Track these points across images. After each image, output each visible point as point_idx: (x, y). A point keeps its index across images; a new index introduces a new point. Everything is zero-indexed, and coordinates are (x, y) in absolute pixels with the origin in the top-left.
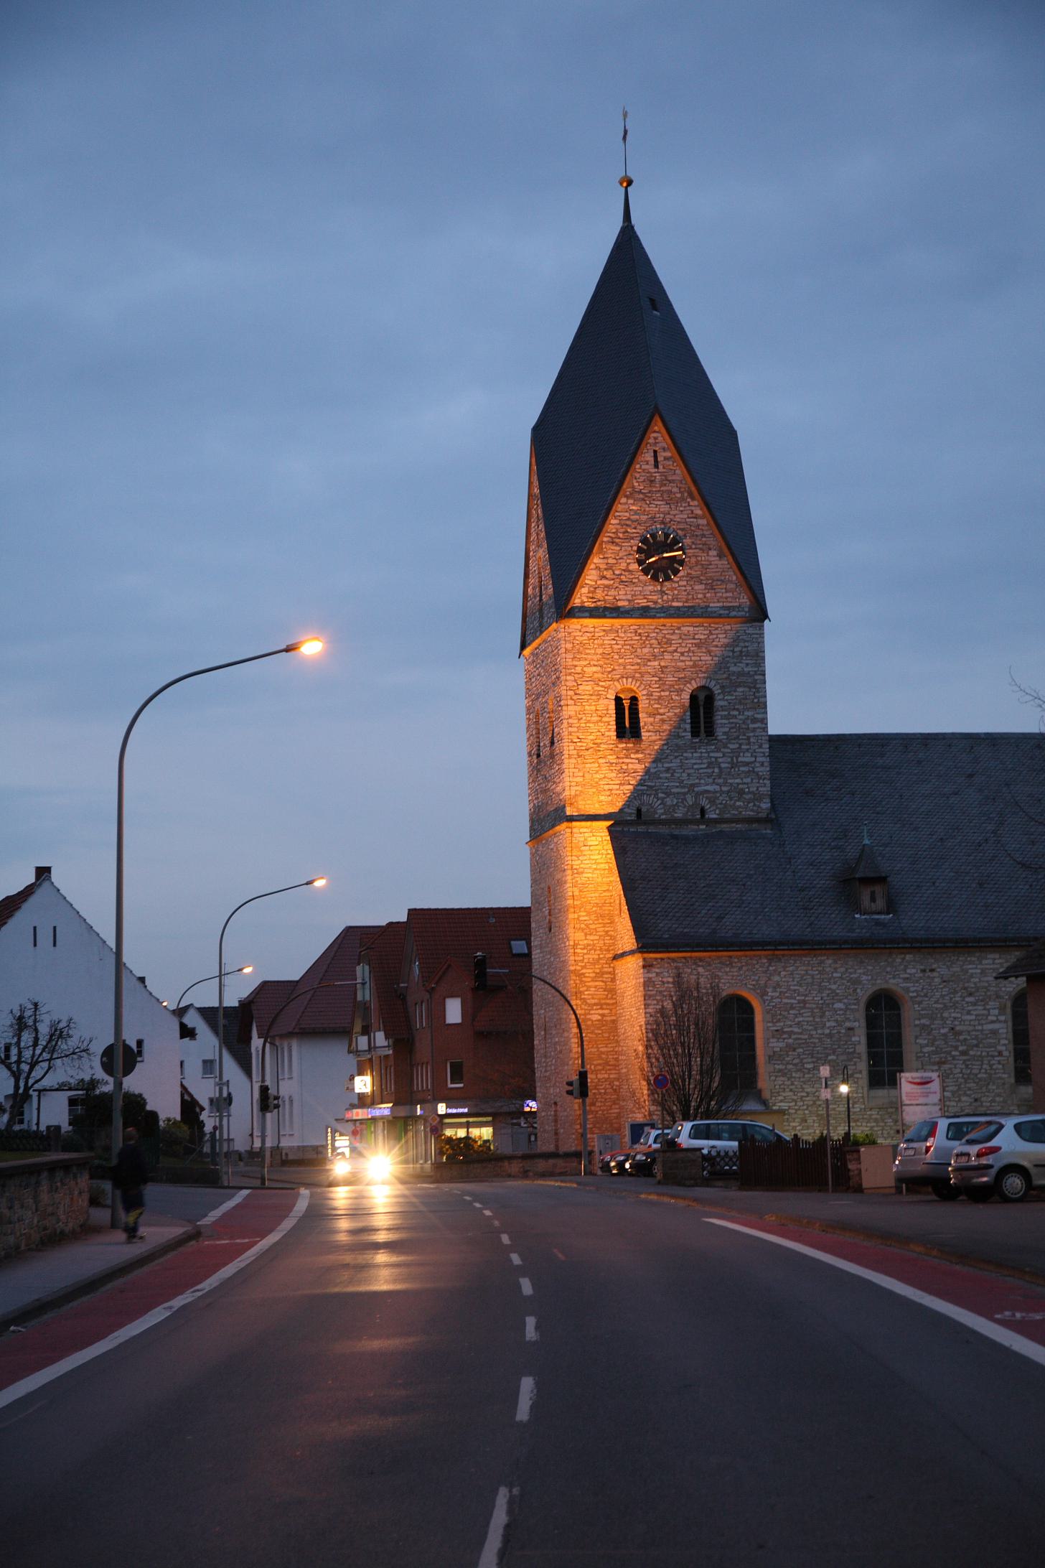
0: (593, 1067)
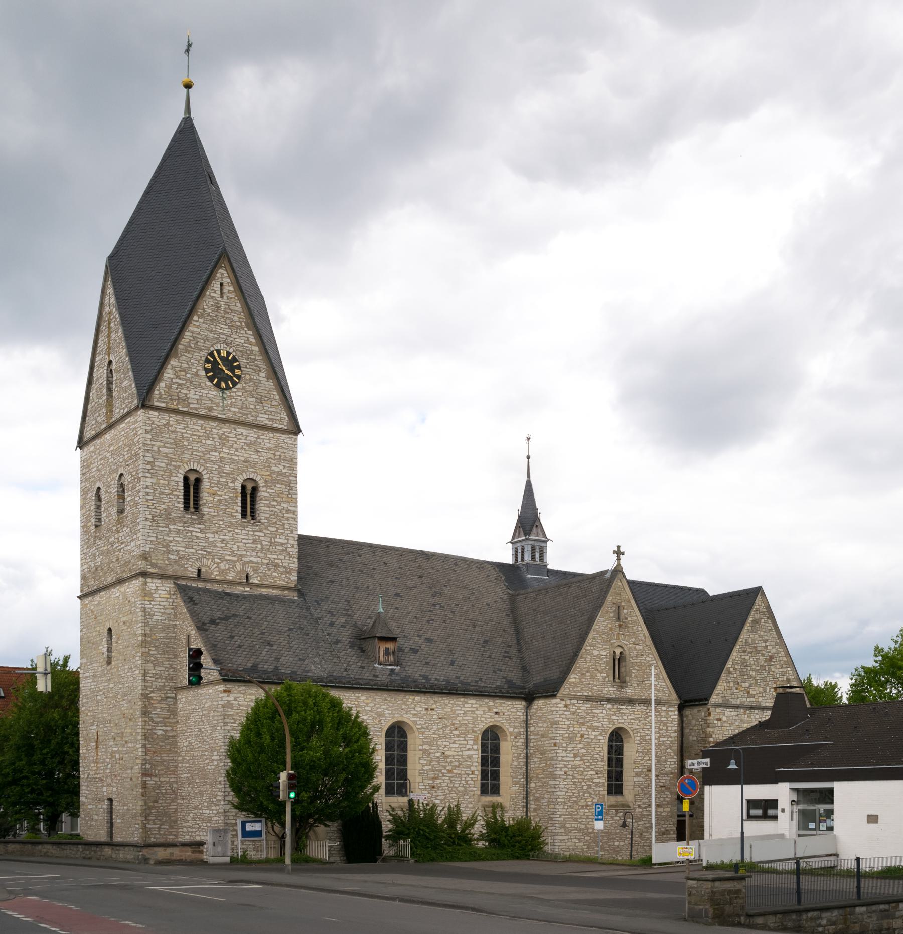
0: (157, 772)
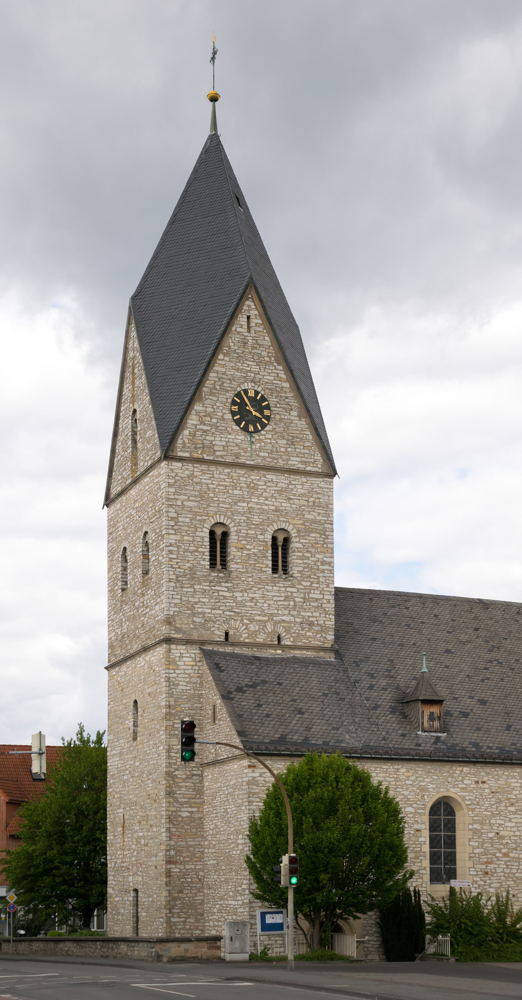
0: (182, 858)
